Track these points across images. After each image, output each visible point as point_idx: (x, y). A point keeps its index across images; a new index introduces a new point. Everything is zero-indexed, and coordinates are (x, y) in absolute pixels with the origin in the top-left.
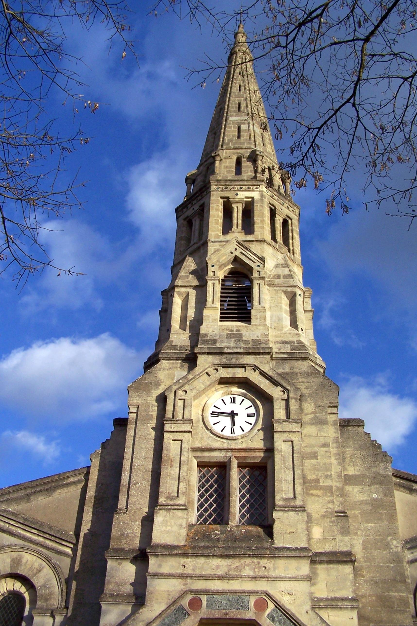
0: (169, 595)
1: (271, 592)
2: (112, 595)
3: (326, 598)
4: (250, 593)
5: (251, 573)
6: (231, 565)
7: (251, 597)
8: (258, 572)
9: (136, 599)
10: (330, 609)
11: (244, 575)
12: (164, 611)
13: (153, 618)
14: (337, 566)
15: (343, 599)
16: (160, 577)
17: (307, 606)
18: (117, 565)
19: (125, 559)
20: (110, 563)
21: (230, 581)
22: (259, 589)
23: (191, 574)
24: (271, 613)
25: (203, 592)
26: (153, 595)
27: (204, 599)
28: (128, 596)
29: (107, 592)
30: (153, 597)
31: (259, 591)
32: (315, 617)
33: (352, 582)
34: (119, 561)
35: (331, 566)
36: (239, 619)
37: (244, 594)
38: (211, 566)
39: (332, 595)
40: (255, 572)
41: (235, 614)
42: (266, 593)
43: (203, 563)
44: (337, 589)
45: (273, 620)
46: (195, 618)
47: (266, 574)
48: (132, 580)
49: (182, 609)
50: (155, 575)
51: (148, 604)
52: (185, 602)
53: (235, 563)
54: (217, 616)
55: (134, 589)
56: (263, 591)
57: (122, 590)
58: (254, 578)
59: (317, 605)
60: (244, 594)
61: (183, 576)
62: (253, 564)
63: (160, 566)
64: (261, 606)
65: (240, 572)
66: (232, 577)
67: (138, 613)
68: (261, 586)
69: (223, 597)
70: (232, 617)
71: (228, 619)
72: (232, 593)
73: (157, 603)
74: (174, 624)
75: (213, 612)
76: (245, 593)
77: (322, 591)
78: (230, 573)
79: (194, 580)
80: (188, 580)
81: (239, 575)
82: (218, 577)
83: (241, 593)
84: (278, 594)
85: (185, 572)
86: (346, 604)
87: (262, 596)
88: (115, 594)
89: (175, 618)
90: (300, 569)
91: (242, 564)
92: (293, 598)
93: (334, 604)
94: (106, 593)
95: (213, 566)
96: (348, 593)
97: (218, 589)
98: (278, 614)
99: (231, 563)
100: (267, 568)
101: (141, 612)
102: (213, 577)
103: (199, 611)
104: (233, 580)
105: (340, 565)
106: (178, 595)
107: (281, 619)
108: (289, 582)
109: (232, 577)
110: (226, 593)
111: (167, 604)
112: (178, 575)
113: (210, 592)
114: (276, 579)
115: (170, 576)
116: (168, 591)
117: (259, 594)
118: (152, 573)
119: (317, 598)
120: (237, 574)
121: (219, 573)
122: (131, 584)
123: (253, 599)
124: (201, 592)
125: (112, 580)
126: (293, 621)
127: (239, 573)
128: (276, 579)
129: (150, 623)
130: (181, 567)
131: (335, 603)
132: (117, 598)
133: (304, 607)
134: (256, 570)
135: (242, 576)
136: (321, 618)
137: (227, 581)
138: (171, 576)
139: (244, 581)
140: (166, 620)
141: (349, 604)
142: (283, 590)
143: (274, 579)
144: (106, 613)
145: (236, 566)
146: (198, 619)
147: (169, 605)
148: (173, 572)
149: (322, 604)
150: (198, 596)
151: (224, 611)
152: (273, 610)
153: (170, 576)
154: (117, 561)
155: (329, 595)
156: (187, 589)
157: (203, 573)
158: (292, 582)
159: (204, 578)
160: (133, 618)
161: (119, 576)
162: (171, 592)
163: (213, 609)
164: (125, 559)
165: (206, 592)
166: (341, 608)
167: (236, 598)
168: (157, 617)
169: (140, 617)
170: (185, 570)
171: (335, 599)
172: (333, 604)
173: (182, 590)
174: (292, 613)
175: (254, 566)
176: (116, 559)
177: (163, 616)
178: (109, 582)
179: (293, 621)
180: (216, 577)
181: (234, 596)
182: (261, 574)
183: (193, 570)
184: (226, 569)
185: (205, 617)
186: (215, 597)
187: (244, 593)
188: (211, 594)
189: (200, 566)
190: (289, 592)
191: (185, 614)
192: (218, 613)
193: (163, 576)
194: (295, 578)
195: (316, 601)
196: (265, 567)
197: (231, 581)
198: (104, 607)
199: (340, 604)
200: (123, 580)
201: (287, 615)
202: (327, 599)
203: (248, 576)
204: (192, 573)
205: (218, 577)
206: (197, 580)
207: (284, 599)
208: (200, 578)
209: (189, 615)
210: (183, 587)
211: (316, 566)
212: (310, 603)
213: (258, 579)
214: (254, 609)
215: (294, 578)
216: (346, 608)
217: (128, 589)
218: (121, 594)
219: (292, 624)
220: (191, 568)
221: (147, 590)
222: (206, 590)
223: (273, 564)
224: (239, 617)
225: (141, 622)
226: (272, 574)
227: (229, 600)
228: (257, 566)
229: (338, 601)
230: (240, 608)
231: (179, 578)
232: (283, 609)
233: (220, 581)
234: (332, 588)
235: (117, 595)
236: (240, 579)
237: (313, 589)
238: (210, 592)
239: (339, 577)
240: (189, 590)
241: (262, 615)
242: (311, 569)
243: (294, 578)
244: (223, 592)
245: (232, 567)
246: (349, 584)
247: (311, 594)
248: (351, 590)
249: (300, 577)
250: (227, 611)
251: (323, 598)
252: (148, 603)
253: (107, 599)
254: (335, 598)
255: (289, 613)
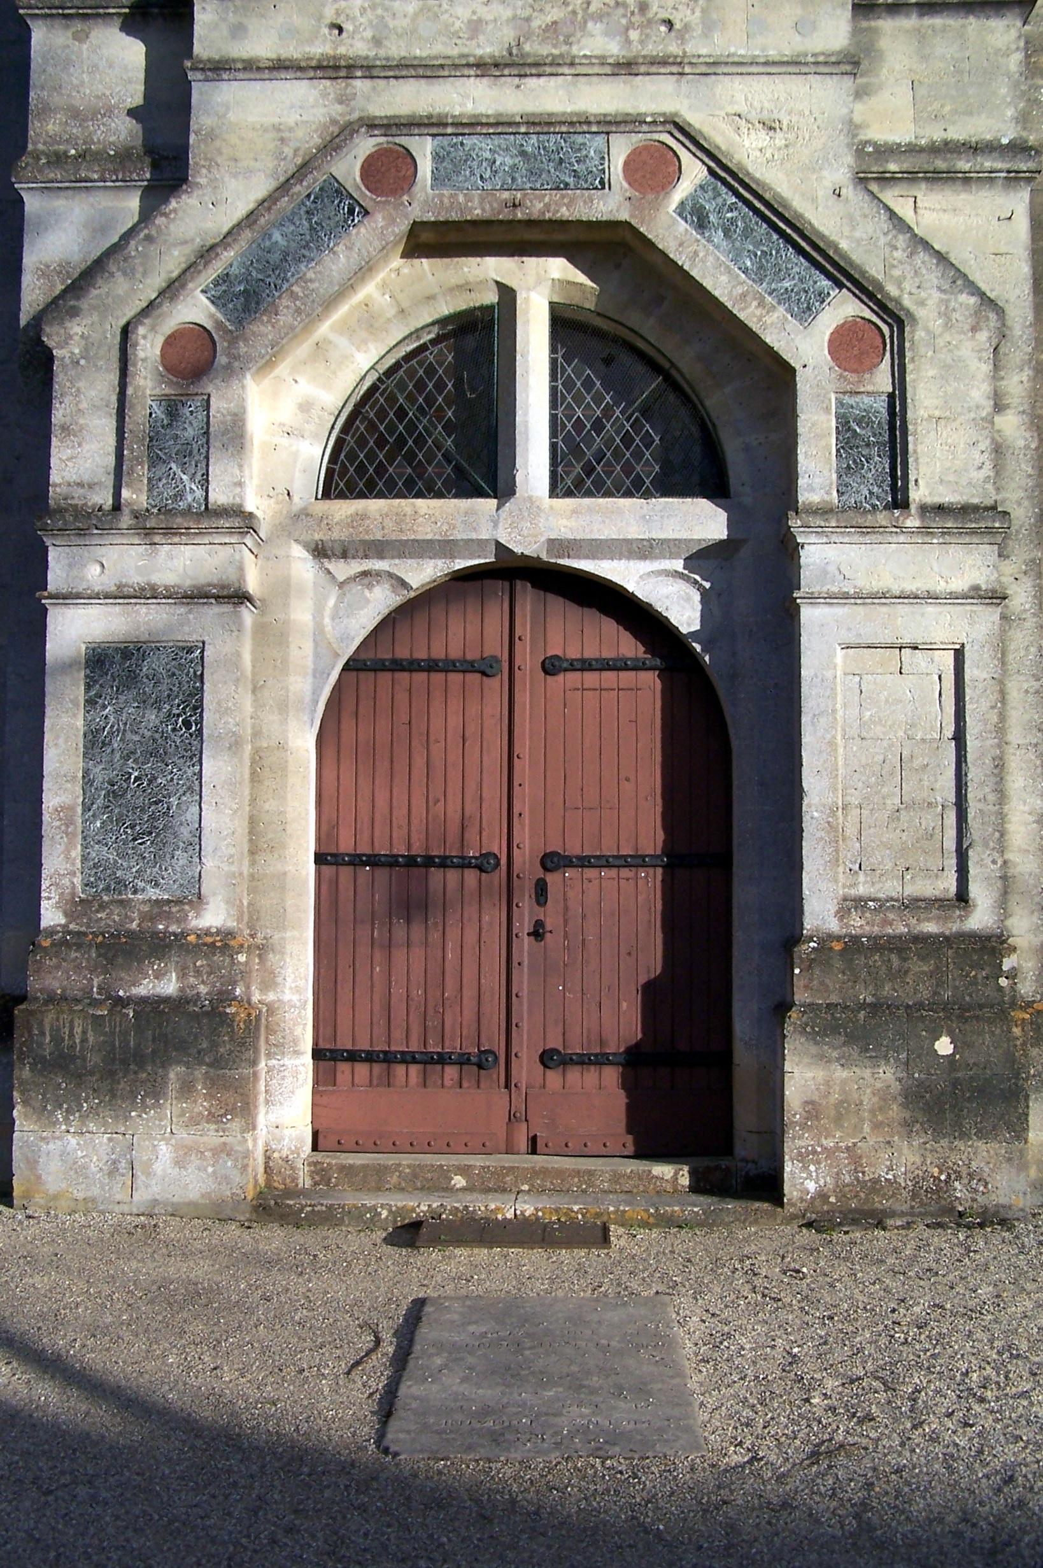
0: (282, 140)
1: (694, 118)
2: (58, 159)
3: (910, 144)
4: (610, 123)
5: (613, 48)
6: (528, 20)
7: (612, 137)
8: (641, 42)
9: (155, 166)
10: (923, 185)
11: (585, 56)
12: (264, 201)
13: (225, 229)
14: (961, 22)
15: (974, 149)
16: (240, 75)
17: (840, 173)
18: (70, 42)
19: (98, 15)
20: (41, 37)
21: (524, 80)
22: (643, 110)
23: (367, 58)
24: (693, 197)
25: (419, 125)
26: (217, 143)
27: (424, 150)
28: (124, 157)
29: (41, 147)
30: (219, 152)
31: (646, 115)
32: (867, 211)
33: (1016, 85)
34: (78, 25)
35: (937, 21)
36: (563, 224)
37: (585, 128)
38: (447, 26)
39: (935, 133)
40: (628, 41)
41: (547, 206)
42: (676, 124)
43: (416, 14)
44: (955, 112)
45: (701, 222)
46: (392, 221)
47: (674, 49)
48: (135, 96)
49: (336, 190)
50: (220, 69)
51: (202, 181)
52: (348, 168)
53: (548, 8)
54: (478, 211)
55: (144, 129)
56: (664, 114)
57: (99, 135)
58: (626, 68)
59: (877, 170)
60: (585, 128)
61: (337, 68)
62: (621, 11)
63: (238, 31)
64: (652, 172)
65: (567, 42)
66: (536, 65)
67: (166, 215)
68: (655, 96)
69: (497, 140)
70: (535, 217)
71: (520, 221)
72: (534, 124)
73: (235, 176)
74: (307, 246)
75: (461, 199)
76: (589, 123)
77: (894, 119)
78: (527, 48)
79: (381, 83)
80: (358, 83)
81: (561, 56)
82: (478, 66)
83: (572, 124)
84: (723, 126)
85: (342, 50)
86: (988, 165)
87: (656, 136)
88: (73, 152)
89: (312, 228)
90: (814, 27)
91: (574, 12)
92: (779, 141)
93: (941, 164)
94: (36, 150)
95: (458, 24)
96: (1000, 124)
97: (478, 112)
98: (720, 200)
99: (529, 11)
100: (678, 26)
101: (175, 211)
102: (456, 66)
103: (405, 198)
104: (539, 75)
105: (972, 19)
106: (317, 140)
107: (732, 221)
108: (765, 78)
109: (536, 65)
110: (510, 124)
111: (274, 174)
112: (314, 63)
113: (446, 125)
114: (714, 67)
115: (280, 67)
116: (277, 128)
117: (645, 128)
118: (209, 60)
119: (875, 144)
120: (556, 52)
121: (479, 52)
122: (132, 113)
123: (621, 149)
124: (411, 125)
125: (56, 100)
126: (781, 225)
127: (564, 48)
128: (714, 67)
129: (212, 247)
130: (326, 31)
131: (945, 160)
132: (78, 168)
133: (825, 173)
134: (634, 35)
135: (574, 57)
136: (892, 214)
137: (516, 80)
138: (286, 68)
139: (582, 79)
140: (277, 236)
141: (999, 165)
142: (742, 108)
143: (704, 69)
144: (43, 225)
145: (549, 19)
146: (404, 226)
147: (282, 179)
148: (292, 51)
149: (893, 167)
150: (397, 140)
151: (506, 195)
152: (701, 187)
153: (280, 67)
154: (67, 27)
155: (921, 132)
156: (355, 116)
157: (418, 52)
158: (776, 78)
159: (421, 72)
160: (146, 231)
161: (82, 83)
162: (291, 130)
163: (459, 189)
164: (98, 15)
165: (432, 125)
166: (967, 180)
167: (551, 146)
168: (238, 226)
169: (172, 227)
170: (341, 43)
171: (947, 148)
172: (939, 165)
173: (334, 122)
174: (777, 195)
175: (624, 21)
176: (65, 16)
177: (262, 221)
178: (47, 110)
179: (781, 225)
180: (468, 65)
181: (542, 137)
182: (652, 49)
183: (377, 42)
184: (508, 35)
185: (430, 217)
186: (468, 141)
187: (580, 124)
188: (449, 130)
189: (402, 23)
190: (765, 116)
191: (351, 211)
192: (481, 203)
193: (252, 69)
194: (795, 65)
195: (869, 154)
196: (669, 24)
197: (532, 82)
198: (33, 203)
199: (963, 165)
200: (97, 97)
201: (758, 205)
202: (912, 149)
203: (602, 61)
204: (372, 54)
205: (478, 66)
206: (393, 82)
207: (747, 143)
208: (404, 73)
209: (367, 213)
210: (339, 108)
211: (873, 24)
212: (849, 159)
213: (642, 69)
214: (625, 185)
215: (787, 63)
216: (988, 179)
217: (122, 131)
218: (98, 153)
219: (775, 237)
220: (369, 34)
221: (193, 126)
222: (430, 117)
223: (703, 11)
224: (564, 213)
225: (175, 245)
226: (698, 47)
227: (523, 153)
228: (637, 19)
229: (960, 153)
230: (571, 180)
231: (319, 73)
232: (742, 182)
233: (485, 80)
234: (936, 105)
235: (82, 156)
236: (566, 70)
237: (860, 111)
238: (446, 125)
239: (966, 66)
240: (361, 119)
241: (656, 206)
242: (856, 32)
243: (787, 63)
244: (498, 124)
245: (535, 24)
246: (1004, 91)
247: (852, 127)
248: (1010, 113)
249: (810, 59)
250: (519, 195)
251: (899, 145)
252: (200, 176)
253: (40, 171)
254: (946, 143)
255: (767, 196)
